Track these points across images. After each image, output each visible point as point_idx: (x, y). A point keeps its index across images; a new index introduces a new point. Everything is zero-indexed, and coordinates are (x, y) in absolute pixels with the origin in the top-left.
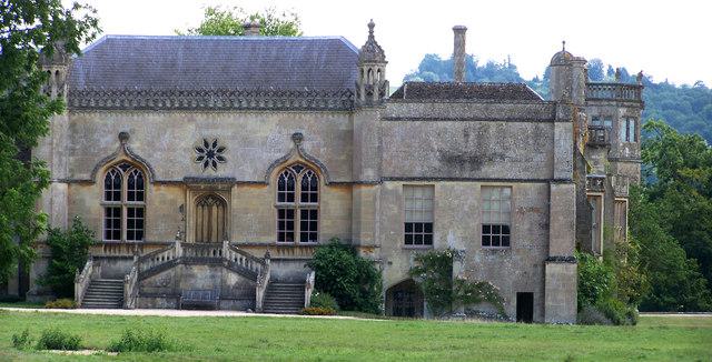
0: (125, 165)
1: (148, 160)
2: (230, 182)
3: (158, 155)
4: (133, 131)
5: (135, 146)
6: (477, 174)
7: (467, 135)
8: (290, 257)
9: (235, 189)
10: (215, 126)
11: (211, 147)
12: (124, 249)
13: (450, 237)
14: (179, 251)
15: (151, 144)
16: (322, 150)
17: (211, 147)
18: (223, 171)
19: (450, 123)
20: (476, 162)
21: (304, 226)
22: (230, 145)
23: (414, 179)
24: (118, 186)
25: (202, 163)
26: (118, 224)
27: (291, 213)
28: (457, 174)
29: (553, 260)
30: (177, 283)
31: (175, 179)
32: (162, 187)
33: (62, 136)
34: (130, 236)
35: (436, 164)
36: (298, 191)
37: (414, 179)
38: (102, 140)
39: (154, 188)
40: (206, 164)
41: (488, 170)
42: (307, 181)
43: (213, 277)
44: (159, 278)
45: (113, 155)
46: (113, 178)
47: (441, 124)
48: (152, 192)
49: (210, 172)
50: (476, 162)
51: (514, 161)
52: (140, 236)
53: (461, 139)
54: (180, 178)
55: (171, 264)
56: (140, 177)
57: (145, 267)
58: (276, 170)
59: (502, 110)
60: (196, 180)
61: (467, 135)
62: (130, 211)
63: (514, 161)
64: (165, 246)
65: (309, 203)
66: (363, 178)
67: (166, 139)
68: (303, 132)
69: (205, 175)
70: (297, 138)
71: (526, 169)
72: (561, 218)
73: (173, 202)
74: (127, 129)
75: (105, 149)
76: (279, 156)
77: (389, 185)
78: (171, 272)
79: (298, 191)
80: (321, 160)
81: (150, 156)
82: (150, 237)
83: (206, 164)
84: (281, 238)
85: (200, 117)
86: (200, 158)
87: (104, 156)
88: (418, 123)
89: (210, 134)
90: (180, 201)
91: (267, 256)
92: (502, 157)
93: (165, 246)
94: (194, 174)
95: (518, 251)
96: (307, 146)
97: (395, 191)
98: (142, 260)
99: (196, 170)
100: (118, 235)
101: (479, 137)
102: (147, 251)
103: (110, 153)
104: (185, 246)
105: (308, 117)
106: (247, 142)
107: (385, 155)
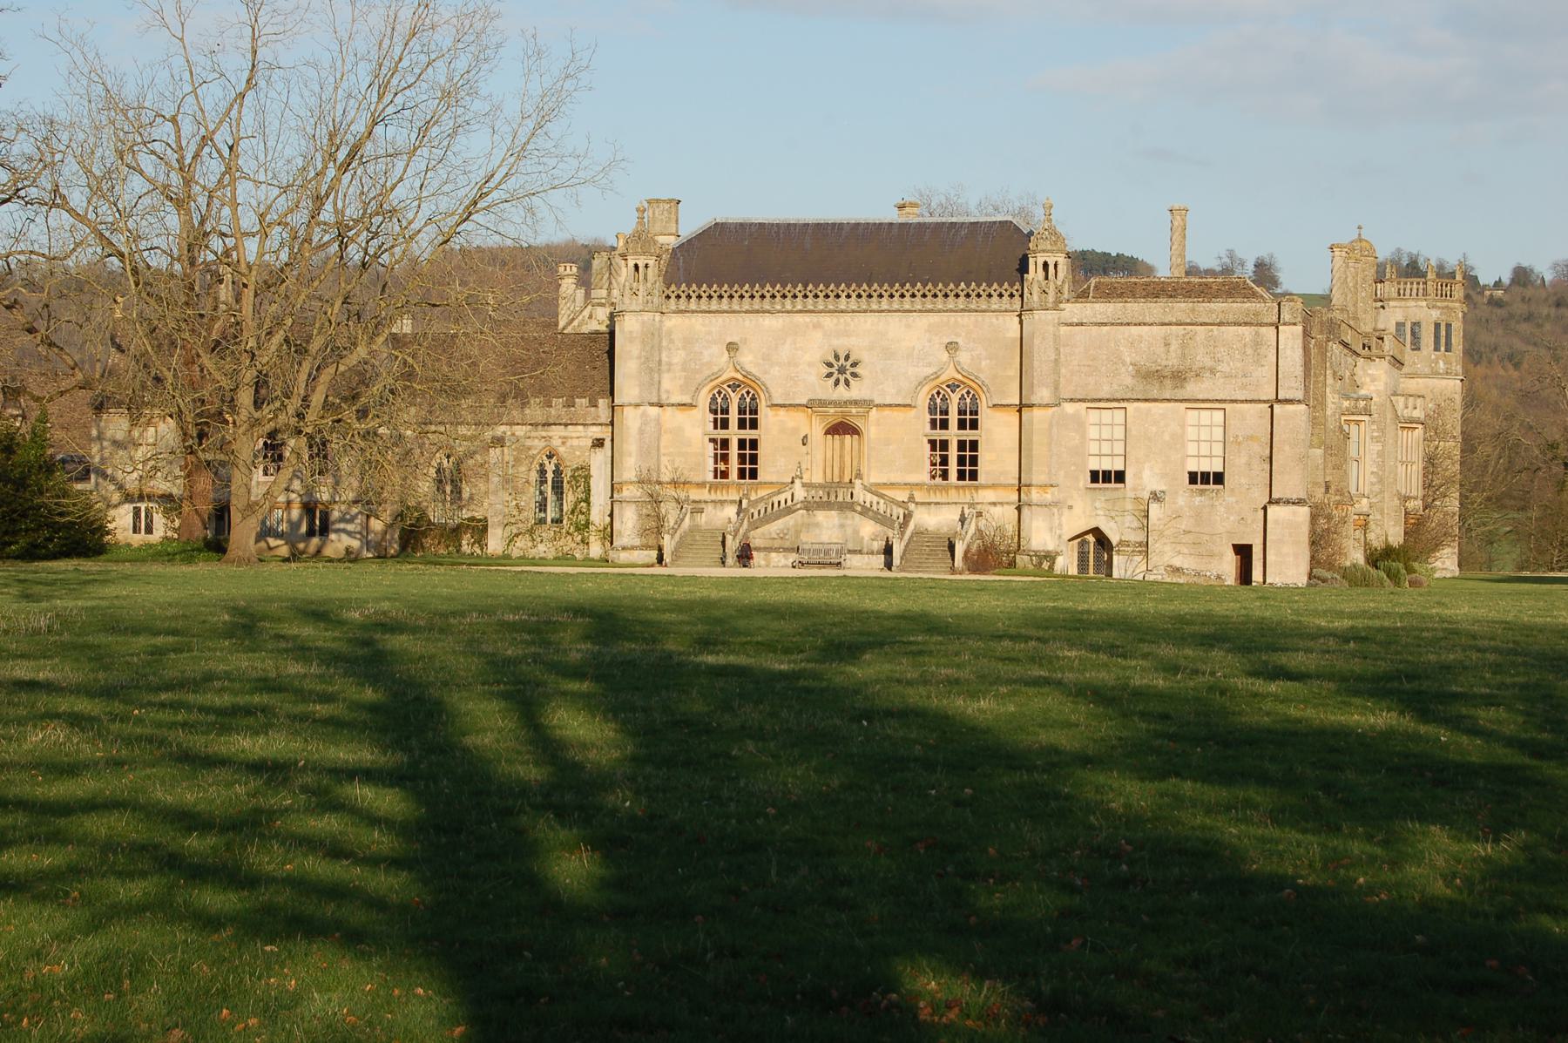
1: (764, 378)
2: (868, 404)
3: (776, 371)
4: (745, 341)
5: (747, 359)
6: (1180, 394)
7: (1167, 345)
8: (943, 500)
11: (842, 361)
13: (1146, 474)
16: (983, 363)
17: (849, 363)
18: (857, 391)
19: (1146, 328)
20: (1179, 377)
21: (961, 461)
22: (865, 356)
26: (944, 461)
28: (1155, 394)
30: (798, 533)
32: (782, 412)
33: (653, 347)
35: (1129, 381)
37: (1100, 400)
39: (770, 412)
40: (837, 383)
41: (1192, 389)
42: (936, 404)
45: (720, 371)
46: (719, 400)
47: (1133, 328)
48: (765, 415)
49: (842, 393)
50: (1179, 377)
51: (1228, 376)
53: (1161, 350)
56: (753, 399)
58: (926, 388)
59: (1212, 311)
60: (823, 403)
61: (1167, 345)
63: (1228, 376)
65: (748, 431)
68: (959, 340)
70: (951, 347)
71: (1244, 387)
72: (1287, 448)
73: (795, 430)
76: (929, 371)
77: (1069, 408)
78: (789, 520)
81: (766, 372)
83: (837, 383)
86: (829, 375)
87: (708, 373)
89: (842, 345)
92: (1213, 371)
94: (822, 395)
95: (1232, 490)
96: (964, 357)
99: (827, 391)
100: (945, 475)
101: (1183, 346)
103: (716, 369)
107: (1063, 371)
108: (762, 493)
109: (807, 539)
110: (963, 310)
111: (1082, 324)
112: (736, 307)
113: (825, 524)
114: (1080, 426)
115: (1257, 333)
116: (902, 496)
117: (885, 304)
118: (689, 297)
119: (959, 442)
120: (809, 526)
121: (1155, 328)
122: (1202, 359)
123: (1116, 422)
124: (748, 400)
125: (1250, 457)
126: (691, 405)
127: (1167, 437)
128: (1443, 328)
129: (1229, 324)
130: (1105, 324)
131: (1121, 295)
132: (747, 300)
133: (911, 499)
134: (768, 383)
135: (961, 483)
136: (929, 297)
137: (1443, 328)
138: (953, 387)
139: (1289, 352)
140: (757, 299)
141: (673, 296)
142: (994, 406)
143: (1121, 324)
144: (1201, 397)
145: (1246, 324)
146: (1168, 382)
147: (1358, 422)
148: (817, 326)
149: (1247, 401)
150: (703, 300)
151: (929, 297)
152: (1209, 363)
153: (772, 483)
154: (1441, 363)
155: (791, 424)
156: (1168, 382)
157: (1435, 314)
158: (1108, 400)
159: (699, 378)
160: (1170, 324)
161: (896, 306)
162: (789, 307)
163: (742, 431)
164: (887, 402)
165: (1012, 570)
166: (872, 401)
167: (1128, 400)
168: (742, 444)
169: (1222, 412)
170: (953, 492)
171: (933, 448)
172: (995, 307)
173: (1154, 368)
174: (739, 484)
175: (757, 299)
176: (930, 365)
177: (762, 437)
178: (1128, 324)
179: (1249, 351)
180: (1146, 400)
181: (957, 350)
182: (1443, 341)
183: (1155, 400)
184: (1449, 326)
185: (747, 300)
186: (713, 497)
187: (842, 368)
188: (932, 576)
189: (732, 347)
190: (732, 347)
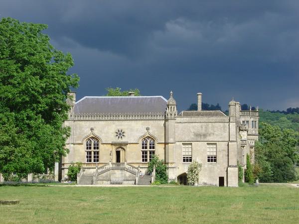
0: (93, 138)
2: (126, 144)
3: (103, 135)
5: (96, 133)
6: (205, 140)
7: (202, 127)
9: (128, 145)
10: (121, 125)
14: (111, 166)
18: (124, 140)
20: (205, 136)
21: (95, 157)
22: (126, 131)
25: (117, 137)
26: (90, 157)
28: (199, 139)
30: (110, 176)
31: (109, 143)
34: (95, 161)
35: (193, 136)
36: (93, 146)
38: (85, 130)
43: (122, 174)
44: (104, 175)
47: (193, 124)
48: (101, 146)
49: (120, 140)
50: (205, 136)
52: (98, 161)
54: (111, 143)
55: (108, 170)
57: (100, 171)
61: (202, 127)
62: (150, 153)
64: (106, 164)
66: (170, 141)
67: (106, 129)
70: (148, 129)
71: (221, 138)
73: (108, 150)
74: (93, 127)
75: (86, 133)
77: (178, 143)
79: (93, 146)
82: (101, 161)
84: (143, 161)
85: (116, 122)
89: (120, 128)
90: (111, 150)
91: (139, 167)
92: (213, 134)
93: (106, 164)
96: (151, 131)
97: (179, 145)
98: (99, 169)
100: (90, 161)
101: (206, 128)
104: (113, 164)
106: (132, 130)
114: (181, 148)
116: (136, 166)
122: (210, 131)
127: (202, 150)
144: (210, 140)
146: (202, 137)
148: (114, 124)
152: (212, 132)
156: (202, 137)
170: (93, 165)
171: (143, 153)
173: (198, 133)
176: (142, 133)
179: (222, 129)
181: (149, 129)
186: (87, 167)
190: (92, 129)
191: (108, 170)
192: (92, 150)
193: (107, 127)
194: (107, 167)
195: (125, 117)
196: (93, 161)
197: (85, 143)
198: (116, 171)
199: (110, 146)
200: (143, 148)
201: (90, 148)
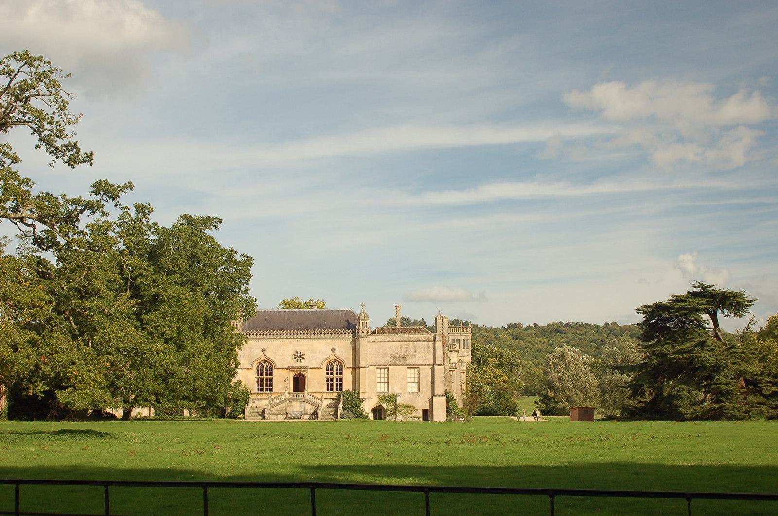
2: (306, 368)
3: (278, 357)
5: (269, 354)
9: (309, 370)
12: (264, 395)
15: (275, 353)
17: (301, 355)
18: (304, 363)
19: (394, 343)
20: (405, 358)
22: (306, 353)
23: (381, 365)
24: (262, 370)
26: (262, 385)
27: (332, 380)
28: (398, 363)
29: (436, 396)
30: (286, 409)
34: (267, 390)
35: (390, 359)
37: (381, 365)
41: (410, 361)
44: (279, 407)
48: (275, 371)
49: (299, 364)
50: (405, 358)
52: (271, 390)
55: (284, 401)
59: (414, 337)
64: (281, 394)
65: (269, 376)
68: (336, 348)
69: (297, 365)
72: (439, 379)
77: (371, 368)
78: (284, 404)
80: (343, 358)
82: (275, 391)
85: (294, 342)
88: (382, 343)
89: (299, 349)
96: (337, 353)
100: (262, 390)
102: (274, 396)
105: (337, 341)
107: (369, 356)
108: (274, 396)
109: (290, 411)
110: (337, 338)
111: (375, 342)
112: (265, 337)
113: (295, 406)
115: (429, 344)
116: (319, 396)
117: (312, 336)
118: (257, 334)
119: (336, 379)
120: (290, 406)
121: (397, 343)
122: (412, 352)
123: (410, 372)
124: (269, 367)
125: (427, 382)
126: (251, 369)
127: (401, 376)
128: (466, 341)
129: (420, 341)
130: (382, 342)
131: (386, 333)
132: (268, 335)
133: (323, 397)
134: (275, 361)
135: (328, 392)
136: (326, 334)
137: (466, 341)
138: (265, 361)
139: (439, 349)
140: (272, 335)
141: (265, 334)
142: (347, 368)
143: (387, 342)
145: (425, 341)
147: (453, 371)
148: (291, 343)
149: (426, 365)
150: (333, 334)
151: (326, 334)
153: (277, 393)
154: (466, 352)
155: (283, 374)
157: (463, 337)
158: (383, 365)
159: (253, 360)
160: (402, 341)
161: (316, 337)
162: (282, 337)
163: (337, 376)
164: (313, 367)
165: (182, 417)
166: (308, 367)
167: (389, 365)
168: (267, 380)
169: (386, 370)
170: (264, 395)
172: (347, 337)
174: (266, 393)
175: (272, 335)
176: (326, 355)
177: (274, 379)
178: (389, 342)
180: (395, 365)
181: (335, 350)
182: (466, 345)
183: (398, 365)
184: (467, 340)
185: (268, 335)
187: (299, 356)
188: (255, 421)
189: (263, 351)
191: (284, 401)
192: (335, 376)
193: (282, 347)
194: (283, 397)
195: (289, 335)
196: (265, 390)
197: (255, 367)
198: (294, 403)
199: (286, 371)
200: (328, 373)
201: (262, 374)
